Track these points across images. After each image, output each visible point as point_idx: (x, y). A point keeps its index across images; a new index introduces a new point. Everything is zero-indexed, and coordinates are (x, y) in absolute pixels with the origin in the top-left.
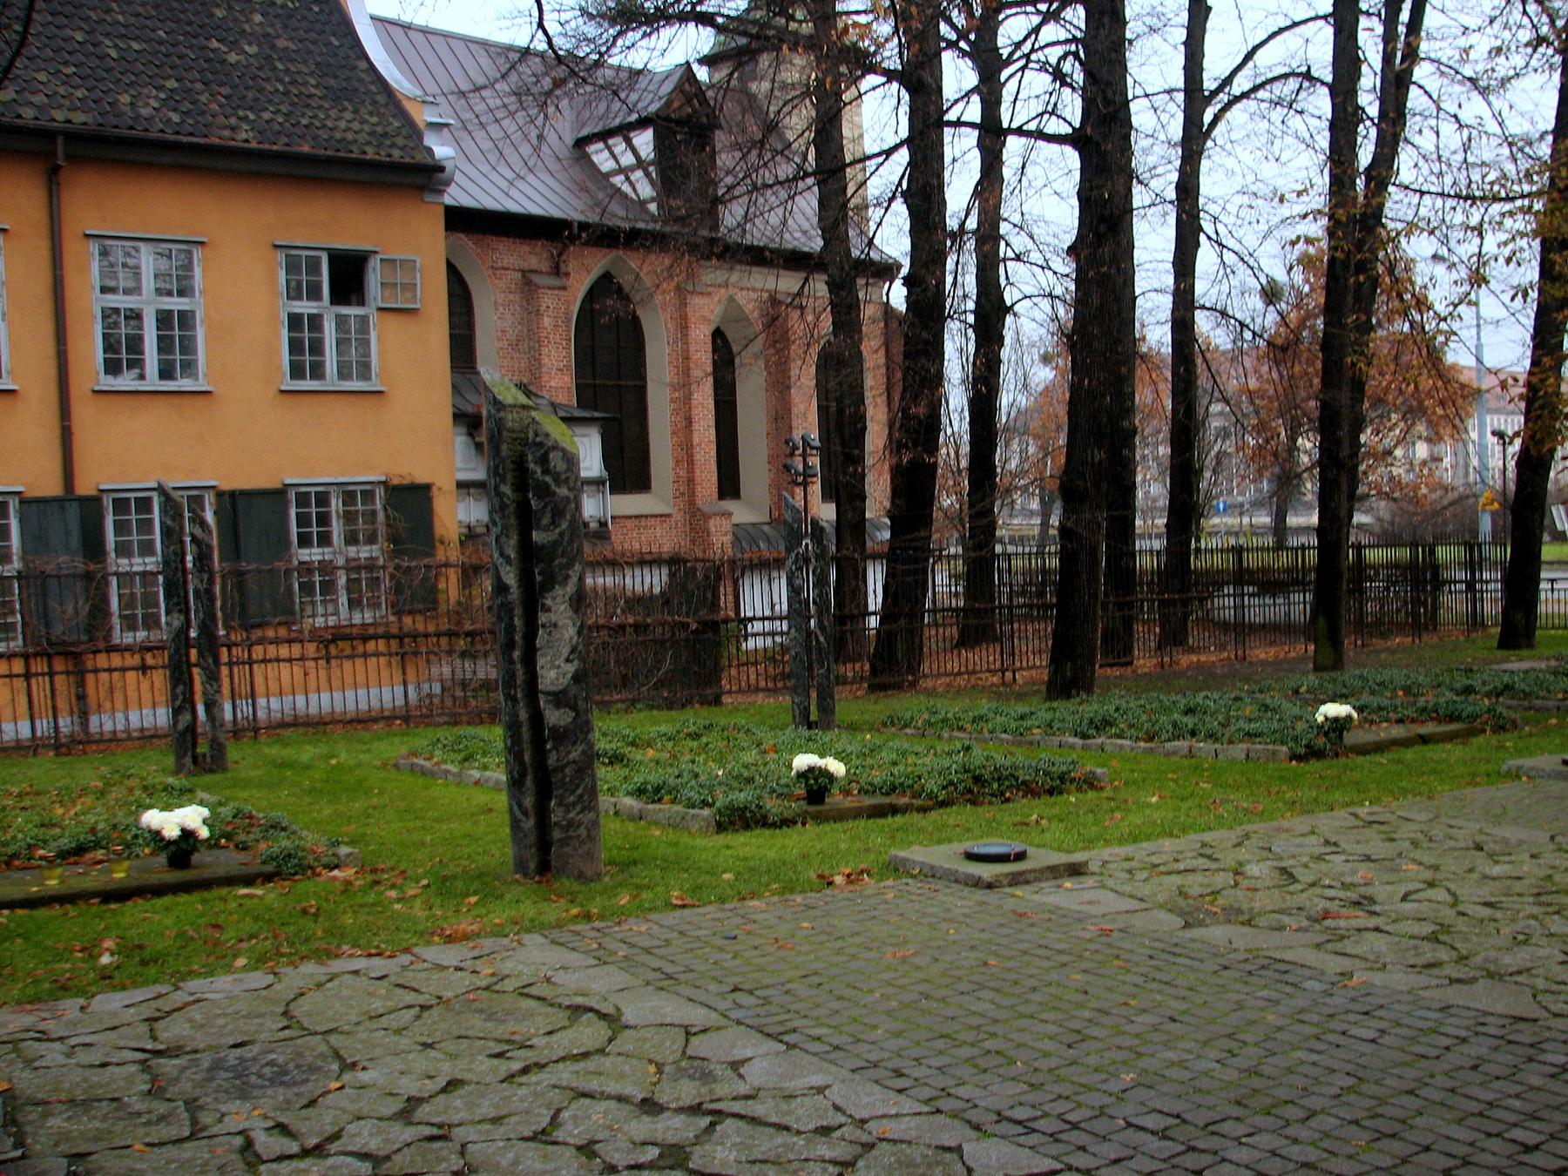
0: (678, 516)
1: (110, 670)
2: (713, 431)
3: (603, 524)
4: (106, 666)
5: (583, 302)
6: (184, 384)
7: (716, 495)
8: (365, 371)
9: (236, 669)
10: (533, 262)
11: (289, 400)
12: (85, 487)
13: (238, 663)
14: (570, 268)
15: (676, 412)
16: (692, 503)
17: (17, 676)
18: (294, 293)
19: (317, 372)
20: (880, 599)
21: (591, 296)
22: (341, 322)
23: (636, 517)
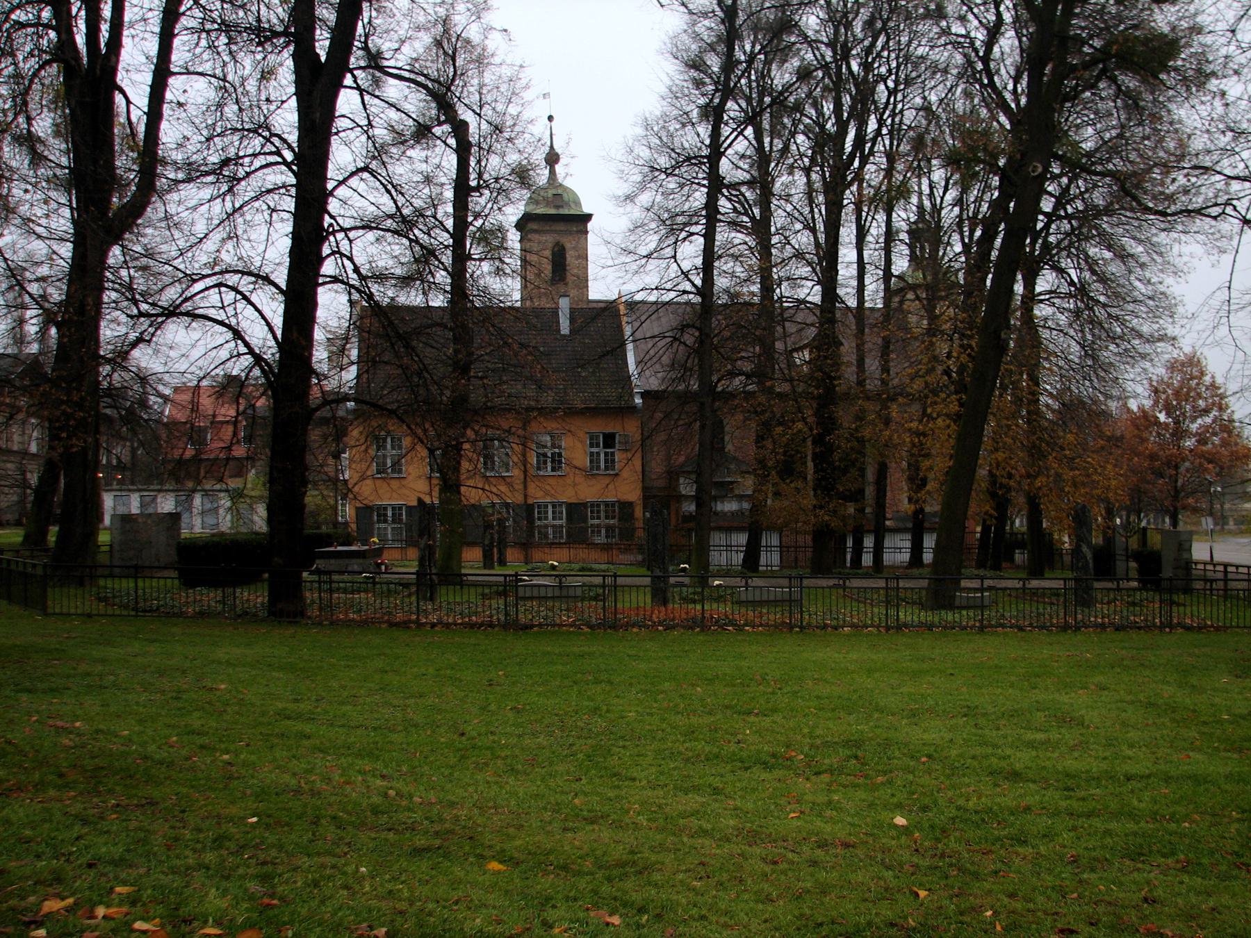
12: (530, 501)
18: (591, 446)
22: (606, 454)
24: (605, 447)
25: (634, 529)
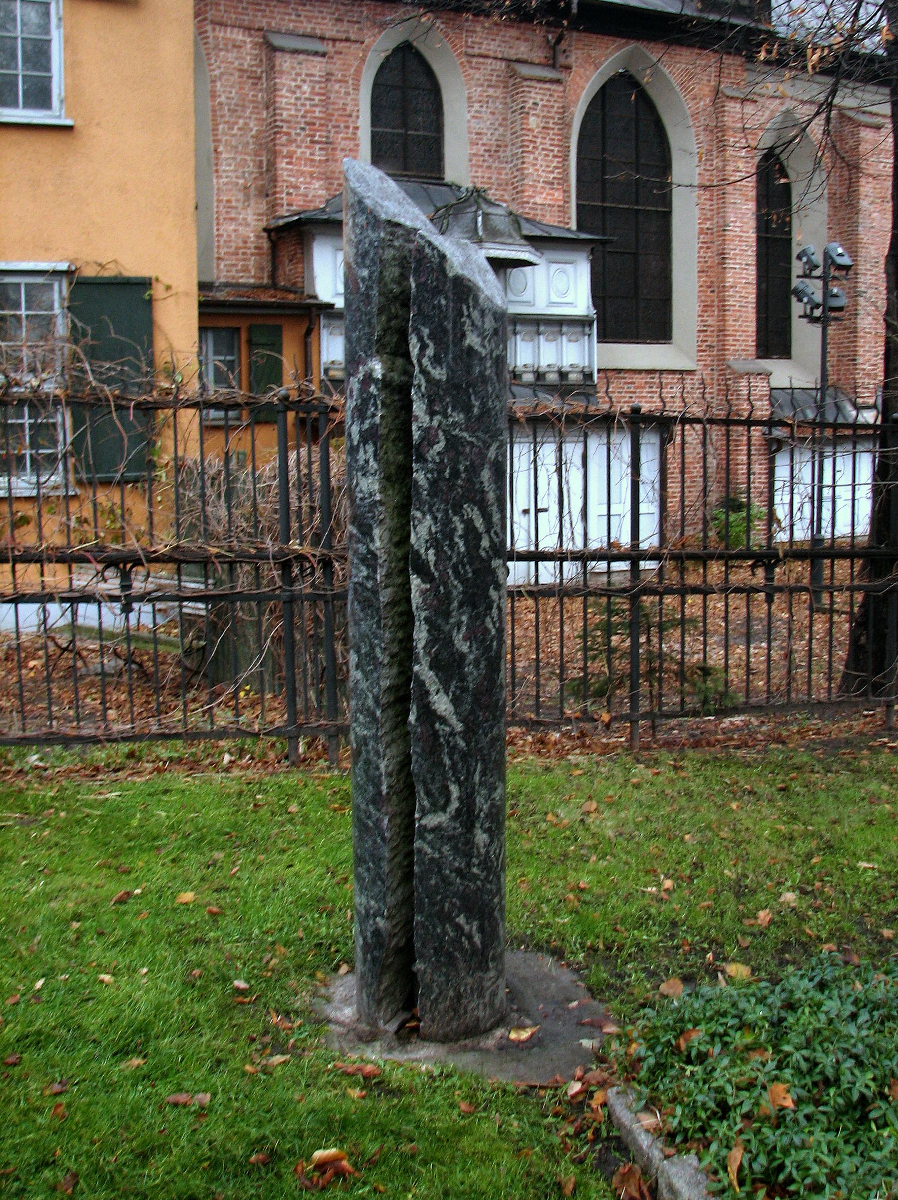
2: (752, 271)
3: (588, 376)
5: (592, 104)
7: (752, 350)
8: (40, 96)
9: (625, 540)
10: (522, 50)
14: (572, 60)
15: (706, 246)
16: (722, 359)
20: (865, 508)
21: (602, 99)
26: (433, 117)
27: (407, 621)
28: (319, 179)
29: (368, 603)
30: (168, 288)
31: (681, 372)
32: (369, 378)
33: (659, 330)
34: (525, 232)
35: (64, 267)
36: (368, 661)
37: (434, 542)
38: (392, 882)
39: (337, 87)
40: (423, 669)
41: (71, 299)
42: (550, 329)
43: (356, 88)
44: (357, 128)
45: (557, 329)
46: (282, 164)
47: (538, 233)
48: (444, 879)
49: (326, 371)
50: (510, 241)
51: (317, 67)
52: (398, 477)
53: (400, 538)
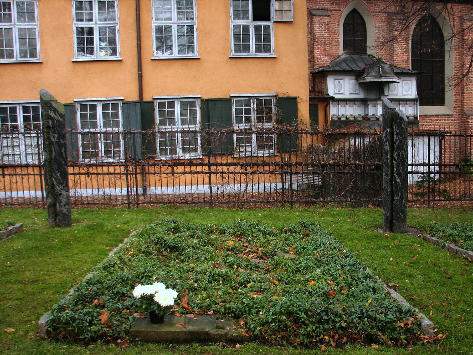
0: (456, 116)
1: (74, 174)
3: (416, 118)
4: (72, 172)
6: (190, 55)
9: (427, 161)
11: (233, 61)
12: (147, 97)
13: (130, 174)
16: (462, 110)
17: (36, 175)
18: (236, 15)
19: (247, 49)
22: (257, 29)
23: (436, 115)
24: (255, 19)
25: (298, 133)
26: (363, 33)
27: (393, 168)
28: (327, 56)
29: (387, 165)
30: (301, 99)
31: (448, 115)
32: (387, 132)
33: (440, 101)
34: (395, 71)
35: (275, 94)
36: (386, 174)
37: (397, 156)
38: (390, 209)
39: (332, 26)
40: (395, 175)
41: (276, 103)
42: (403, 103)
43: (338, 25)
44: (339, 38)
45: (405, 103)
46: (316, 52)
47: (399, 71)
48: (398, 208)
49: (332, 118)
50: (390, 75)
51: (326, 20)
52: (392, 147)
53: (392, 155)
